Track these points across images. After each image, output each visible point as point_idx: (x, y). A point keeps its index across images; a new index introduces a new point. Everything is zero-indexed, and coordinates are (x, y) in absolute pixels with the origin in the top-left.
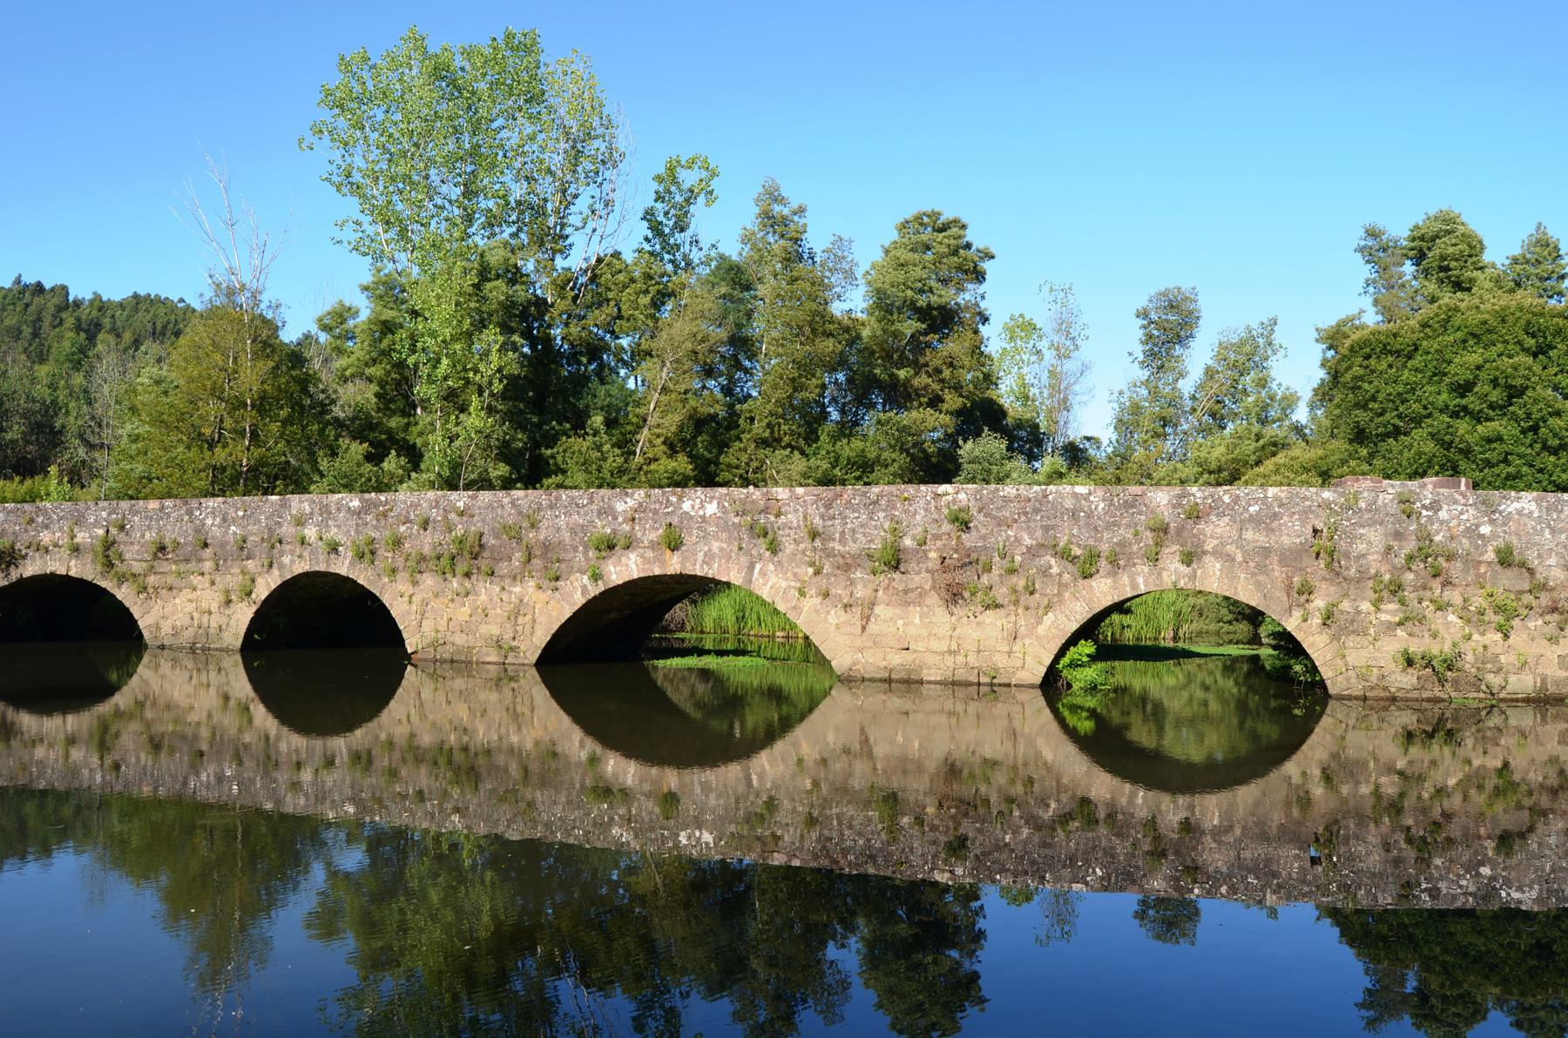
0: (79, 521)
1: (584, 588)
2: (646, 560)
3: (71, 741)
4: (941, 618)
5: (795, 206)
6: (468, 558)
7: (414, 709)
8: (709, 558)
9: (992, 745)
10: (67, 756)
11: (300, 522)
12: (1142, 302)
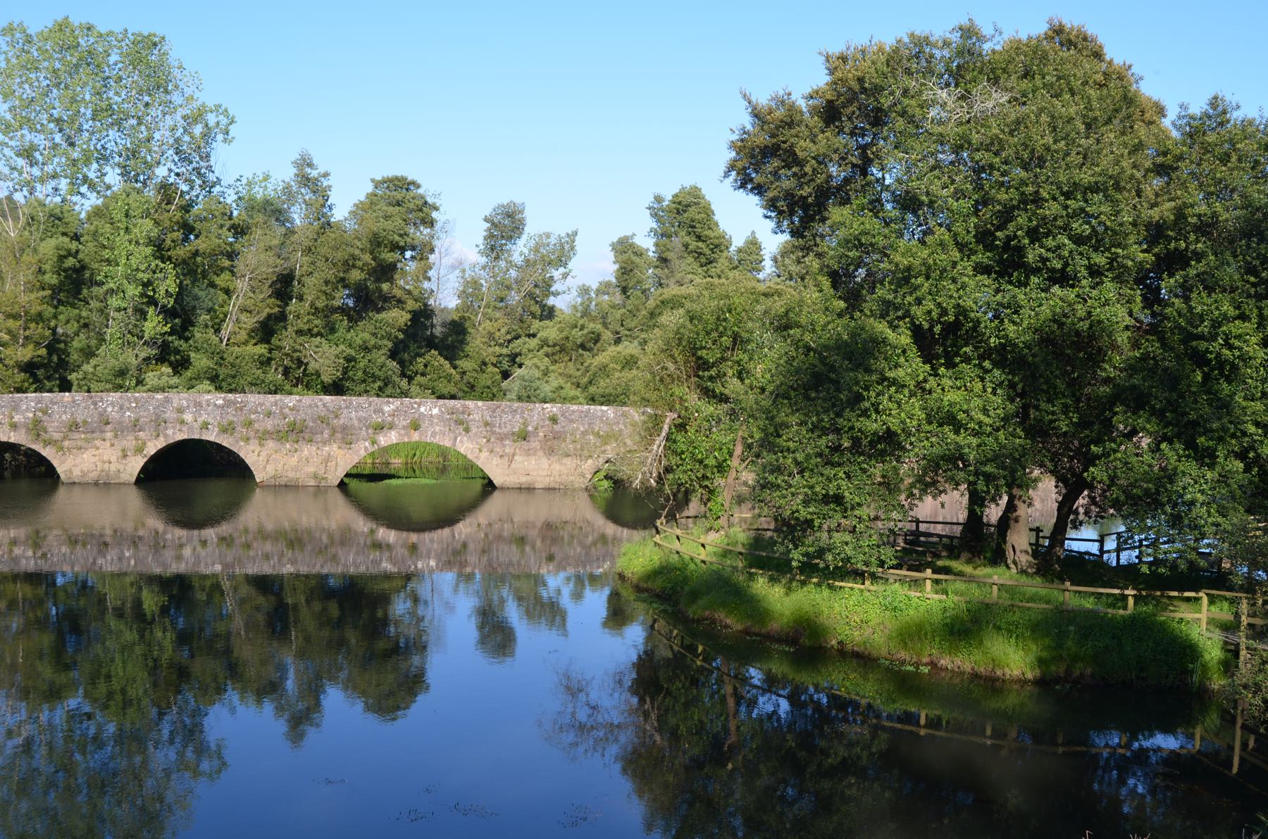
0: (16, 408)
1: (366, 448)
2: (400, 435)
3: (14, 542)
4: (545, 462)
5: (322, 170)
6: (295, 432)
7: (257, 512)
8: (434, 434)
9: (567, 514)
10: (11, 551)
11: (180, 410)
12: (488, 211)
